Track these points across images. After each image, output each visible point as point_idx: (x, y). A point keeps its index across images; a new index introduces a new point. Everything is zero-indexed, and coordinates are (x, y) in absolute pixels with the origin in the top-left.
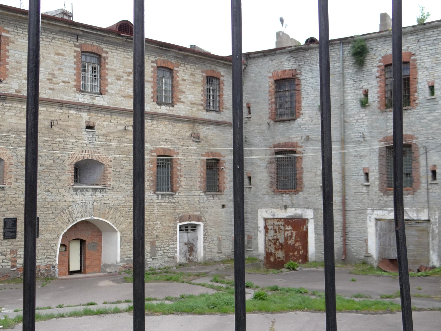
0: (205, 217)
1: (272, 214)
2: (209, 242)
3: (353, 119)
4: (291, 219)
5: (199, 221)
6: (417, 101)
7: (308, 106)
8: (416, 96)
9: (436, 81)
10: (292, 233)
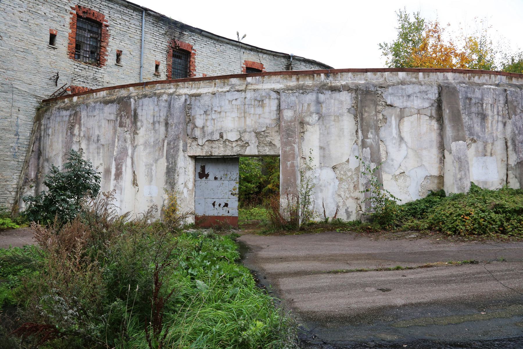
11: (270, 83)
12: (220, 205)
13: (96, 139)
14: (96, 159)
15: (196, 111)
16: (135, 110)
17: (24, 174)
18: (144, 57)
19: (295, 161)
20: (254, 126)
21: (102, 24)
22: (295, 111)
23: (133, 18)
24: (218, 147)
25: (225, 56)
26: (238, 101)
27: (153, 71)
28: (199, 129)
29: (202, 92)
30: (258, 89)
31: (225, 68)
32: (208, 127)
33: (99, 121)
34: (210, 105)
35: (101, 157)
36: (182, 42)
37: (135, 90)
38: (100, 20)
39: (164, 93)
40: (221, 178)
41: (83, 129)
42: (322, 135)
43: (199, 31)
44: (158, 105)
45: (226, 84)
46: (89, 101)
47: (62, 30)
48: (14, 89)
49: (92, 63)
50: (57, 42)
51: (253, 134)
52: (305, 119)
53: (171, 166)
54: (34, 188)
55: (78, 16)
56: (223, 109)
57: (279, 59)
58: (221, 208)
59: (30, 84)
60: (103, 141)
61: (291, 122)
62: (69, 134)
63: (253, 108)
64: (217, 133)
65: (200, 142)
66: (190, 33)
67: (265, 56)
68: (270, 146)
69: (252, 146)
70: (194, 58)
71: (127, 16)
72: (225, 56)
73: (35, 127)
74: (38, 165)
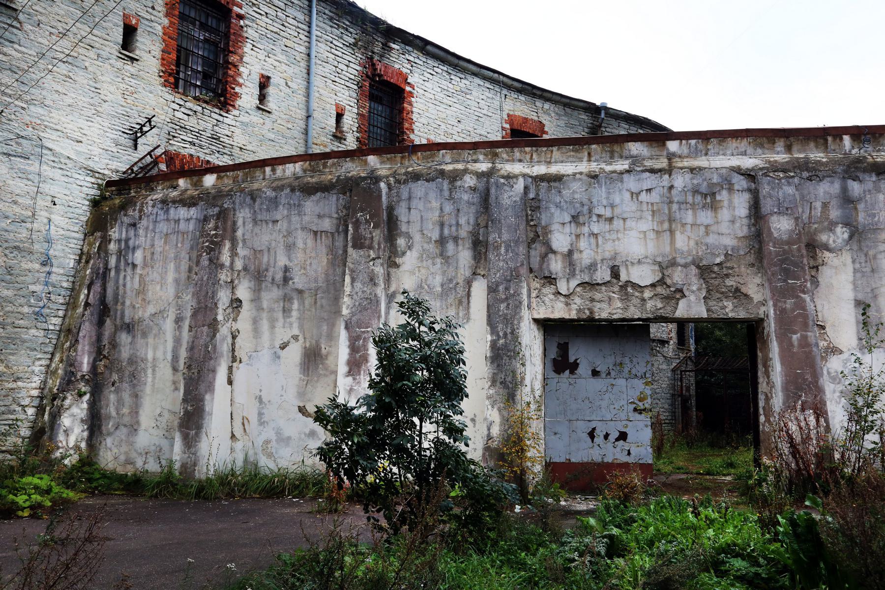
11: (724, 154)
12: (606, 436)
13: (279, 276)
14: (280, 324)
15: (552, 214)
16: (391, 209)
17: (61, 361)
18: (314, 95)
19: (809, 334)
20: (694, 253)
21: (231, 10)
22: (797, 219)
24: (607, 298)
25: (469, 102)
26: (653, 193)
27: (332, 126)
28: (559, 257)
29: (562, 172)
30: (701, 169)
31: (471, 129)
32: (581, 252)
33: (289, 233)
34: (585, 201)
35: (293, 319)
36: (386, 67)
37: (382, 163)
39: (466, 171)
40: (609, 374)
41: (241, 251)
42: (859, 275)
43: (421, 44)
44: (451, 198)
45: (616, 155)
46: (256, 186)
47: (148, 17)
48: (44, 151)
50: (138, 44)
51: (694, 270)
52: (818, 238)
53: (502, 341)
54: (87, 397)
56: (617, 211)
57: (576, 113)
58: (610, 445)
59: (78, 142)
60: (298, 281)
61: (789, 242)
62: (205, 262)
63: (690, 212)
64: (604, 267)
65: (563, 287)
66: (403, 45)
67: (547, 106)
68: (735, 298)
69: (692, 298)
70: (411, 104)
72: (469, 102)
73: (90, 245)
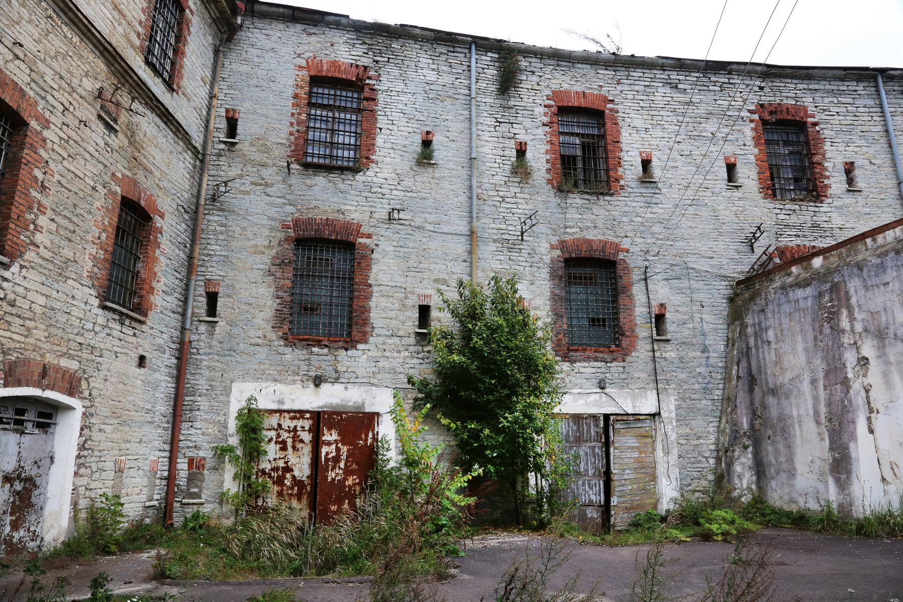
0: (92, 384)
1: (276, 398)
2: (93, 472)
3: (496, 194)
4: (339, 414)
5: (72, 391)
6: (622, 182)
7: (392, 148)
8: (619, 173)
9: (653, 153)
10: (338, 450)
17: (727, 422)
21: (805, 123)
23: (860, 95)
38: (802, 118)
41: (858, 315)
47: (743, 153)
48: (690, 271)
49: (805, 198)
50: (739, 175)
54: (750, 449)
55: (764, 122)
71: (848, 96)
73: (733, 332)
74: (752, 403)
